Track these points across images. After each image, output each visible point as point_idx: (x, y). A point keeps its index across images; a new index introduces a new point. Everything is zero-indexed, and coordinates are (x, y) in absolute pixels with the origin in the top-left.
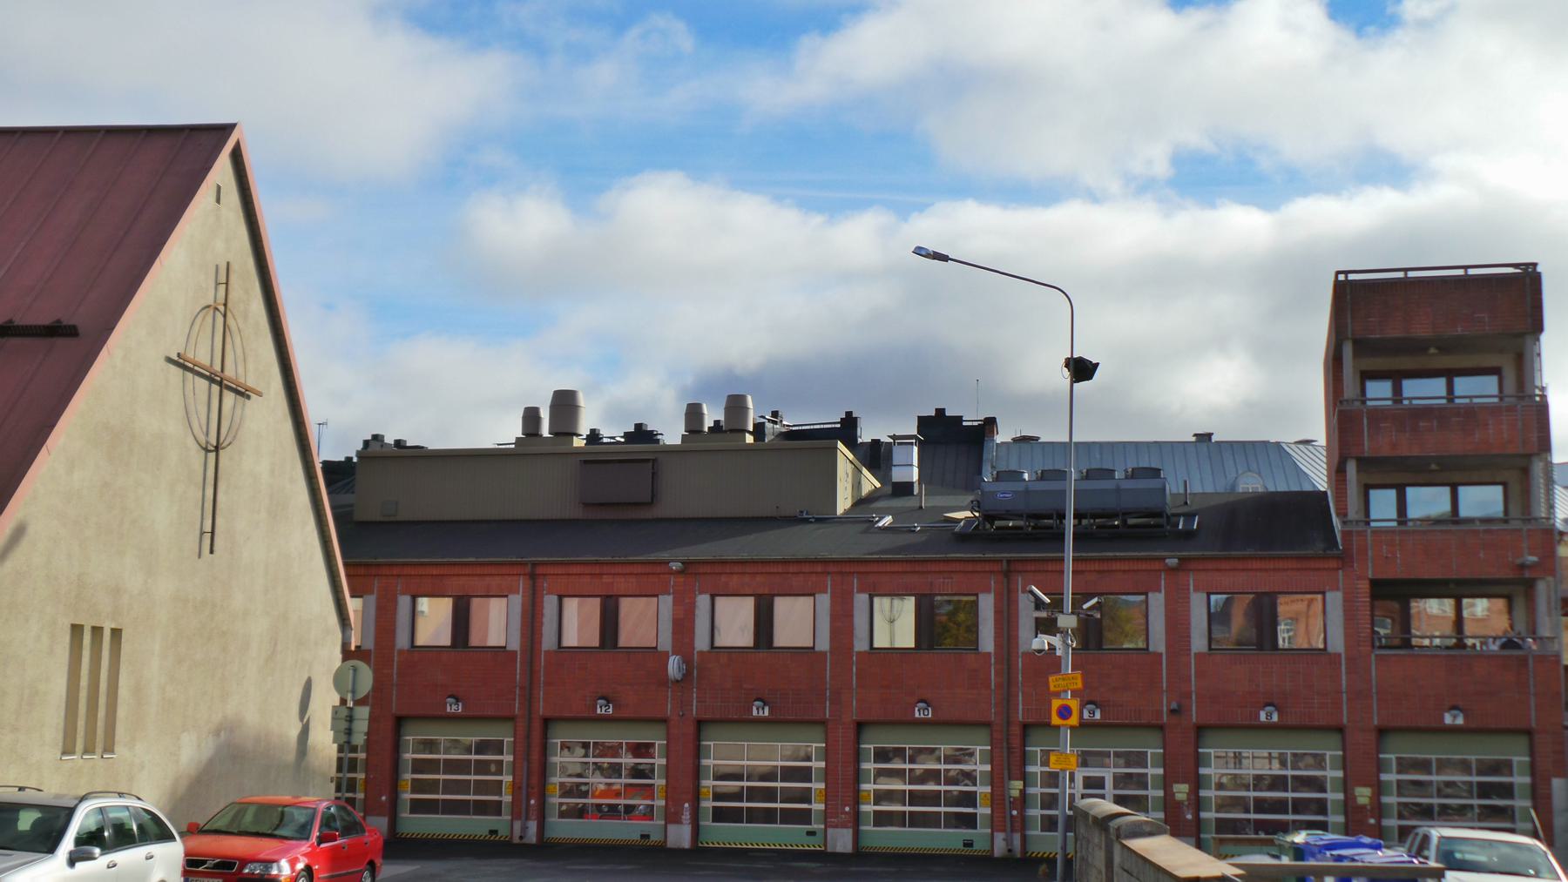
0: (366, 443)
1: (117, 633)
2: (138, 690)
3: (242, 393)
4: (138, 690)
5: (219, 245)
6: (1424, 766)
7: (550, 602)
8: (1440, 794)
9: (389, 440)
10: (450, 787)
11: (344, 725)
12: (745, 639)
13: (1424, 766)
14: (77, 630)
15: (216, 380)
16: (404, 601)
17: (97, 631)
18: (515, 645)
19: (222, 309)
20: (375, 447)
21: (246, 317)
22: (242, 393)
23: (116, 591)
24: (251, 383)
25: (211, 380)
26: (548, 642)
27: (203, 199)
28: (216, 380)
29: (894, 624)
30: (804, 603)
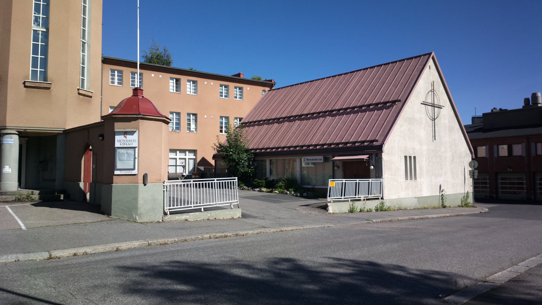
0: (492, 110)
1: (415, 157)
2: (421, 168)
3: (440, 107)
4: (421, 168)
5: (431, 78)
6: (506, 179)
7: (533, 145)
8: (509, 184)
9: (498, 109)
10: (510, 188)
11: (472, 174)
12: (506, 154)
13: (506, 179)
14: (406, 157)
15: (433, 106)
16: (495, 146)
17: (410, 157)
18: (524, 155)
19: (433, 91)
20: (495, 111)
21: (439, 91)
22: (440, 107)
23: (414, 149)
24: (441, 105)
25: (432, 106)
26: (533, 154)
27: (426, 69)
28: (433, 106)
29: (503, 150)
30: (520, 146)
